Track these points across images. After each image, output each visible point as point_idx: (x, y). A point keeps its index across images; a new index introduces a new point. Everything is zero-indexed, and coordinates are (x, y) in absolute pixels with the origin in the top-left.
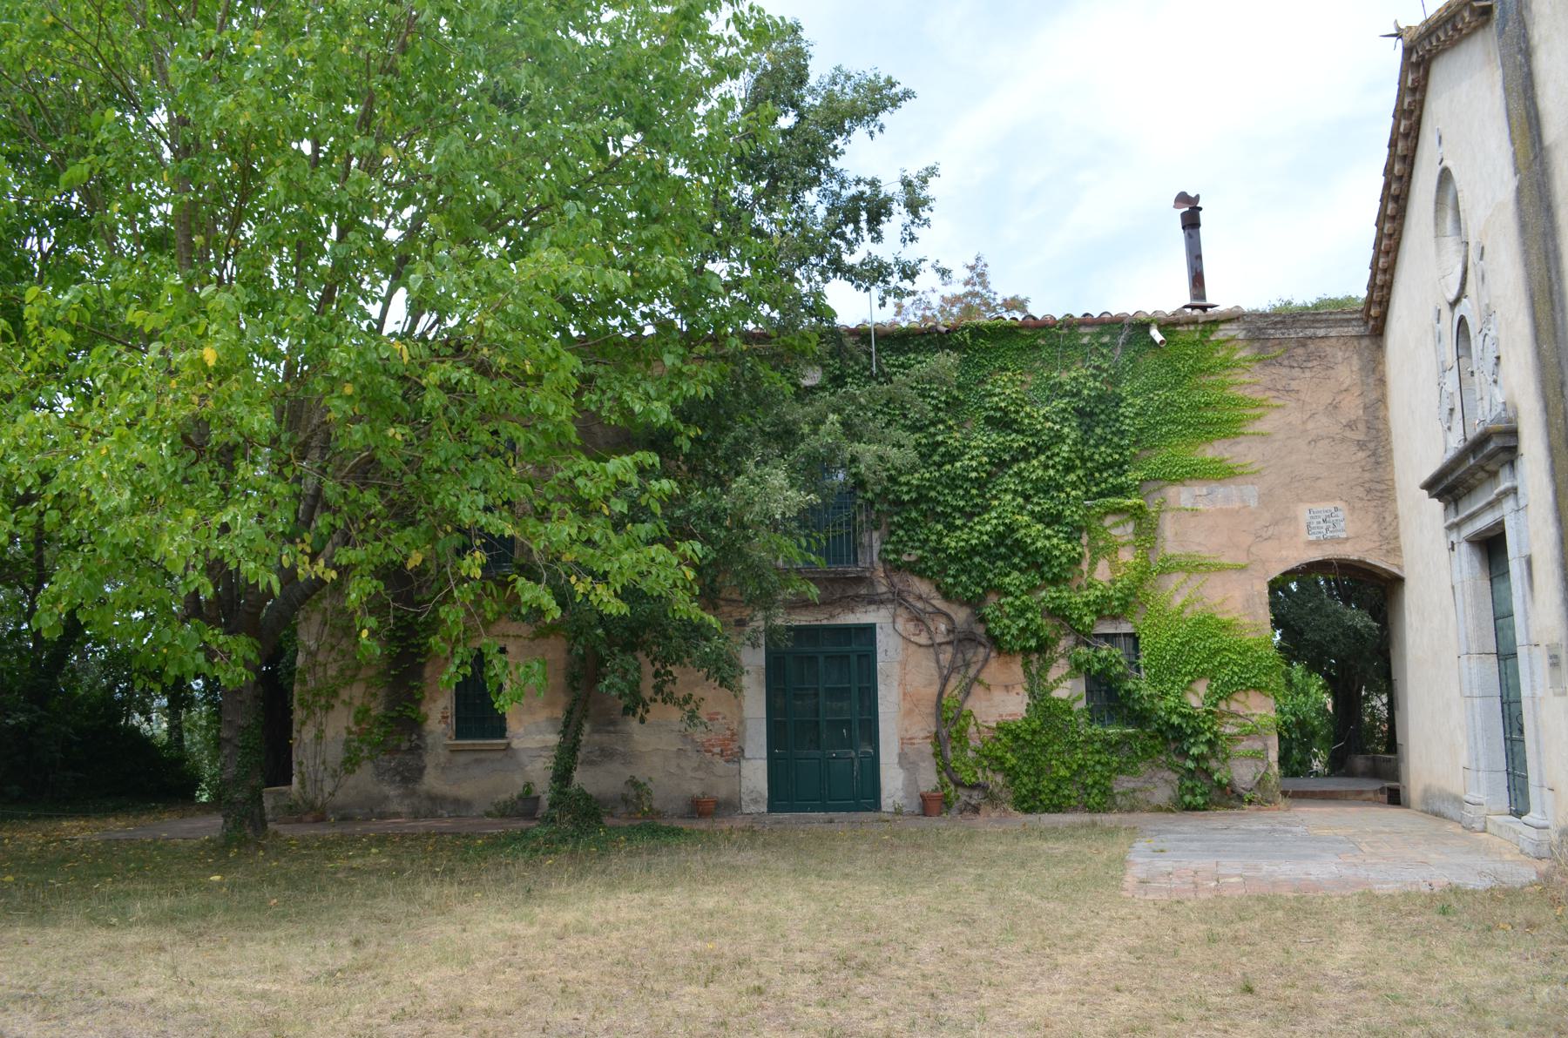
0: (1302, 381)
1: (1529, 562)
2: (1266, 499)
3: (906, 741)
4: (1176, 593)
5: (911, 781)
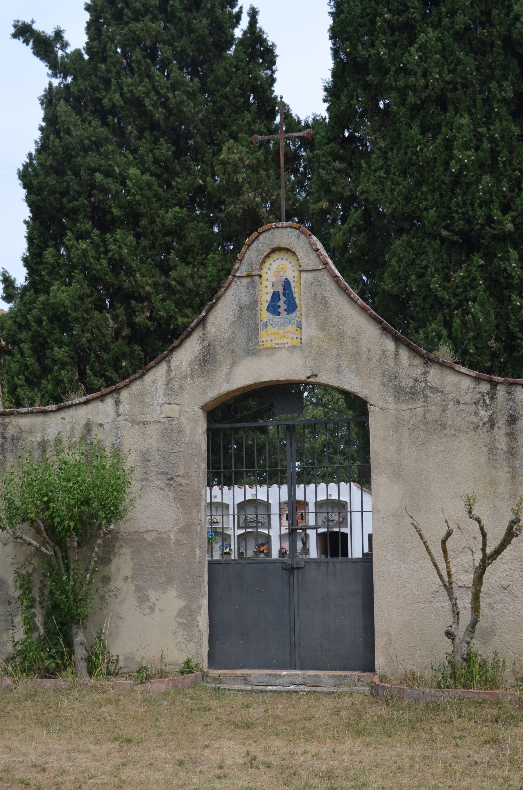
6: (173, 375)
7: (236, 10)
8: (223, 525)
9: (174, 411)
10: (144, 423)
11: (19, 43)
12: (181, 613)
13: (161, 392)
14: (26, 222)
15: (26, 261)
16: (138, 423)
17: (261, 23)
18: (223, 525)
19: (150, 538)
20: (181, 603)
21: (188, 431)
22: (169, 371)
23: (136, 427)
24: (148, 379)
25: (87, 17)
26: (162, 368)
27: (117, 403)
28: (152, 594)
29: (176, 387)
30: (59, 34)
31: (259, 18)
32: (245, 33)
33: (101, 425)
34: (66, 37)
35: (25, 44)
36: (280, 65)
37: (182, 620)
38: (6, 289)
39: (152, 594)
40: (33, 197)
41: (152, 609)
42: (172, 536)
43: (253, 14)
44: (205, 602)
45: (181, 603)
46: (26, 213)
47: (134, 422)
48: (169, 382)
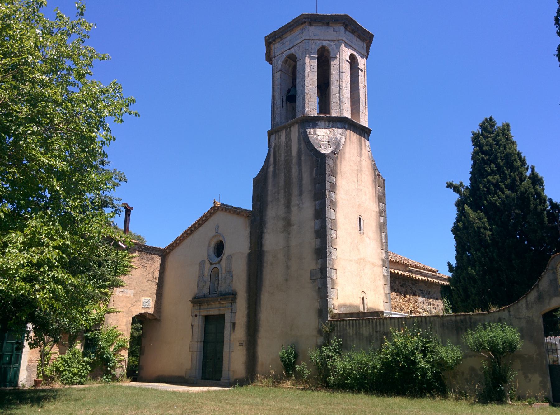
0: (148, 264)
1: (234, 325)
2: (135, 294)
3: (30, 361)
4: (111, 321)
5: (29, 376)
6: (528, 303)
7: (526, 166)
8: (230, 350)
10: (520, 318)
11: (448, 189)
12: (541, 382)
13: (525, 308)
14: (455, 246)
15: (456, 258)
16: (518, 318)
17: (536, 170)
18: (230, 350)
19: (526, 356)
20: (541, 379)
21: (536, 321)
22: (527, 301)
23: (517, 320)
24: (519, 304)
26: (524, 300)
27: (509, 312)
28: (530, 376)
29: (530, 307)
30: (461, 184)
31: (535, 169)
32: (530, 175)
33: (504, 319)
34: (464, 184)
35: (446, 185)
36: (545, 184)
37: (542, 385)
38: (449, 268)
39: (530, 376)
40: (456, 238)
41: (530, 380)
42: (534, 356)
43: (533, 169)
44: (549, 378)
45: (541, 379)
46: (454, 242)
47: (516, 318)
48: (527, 305)
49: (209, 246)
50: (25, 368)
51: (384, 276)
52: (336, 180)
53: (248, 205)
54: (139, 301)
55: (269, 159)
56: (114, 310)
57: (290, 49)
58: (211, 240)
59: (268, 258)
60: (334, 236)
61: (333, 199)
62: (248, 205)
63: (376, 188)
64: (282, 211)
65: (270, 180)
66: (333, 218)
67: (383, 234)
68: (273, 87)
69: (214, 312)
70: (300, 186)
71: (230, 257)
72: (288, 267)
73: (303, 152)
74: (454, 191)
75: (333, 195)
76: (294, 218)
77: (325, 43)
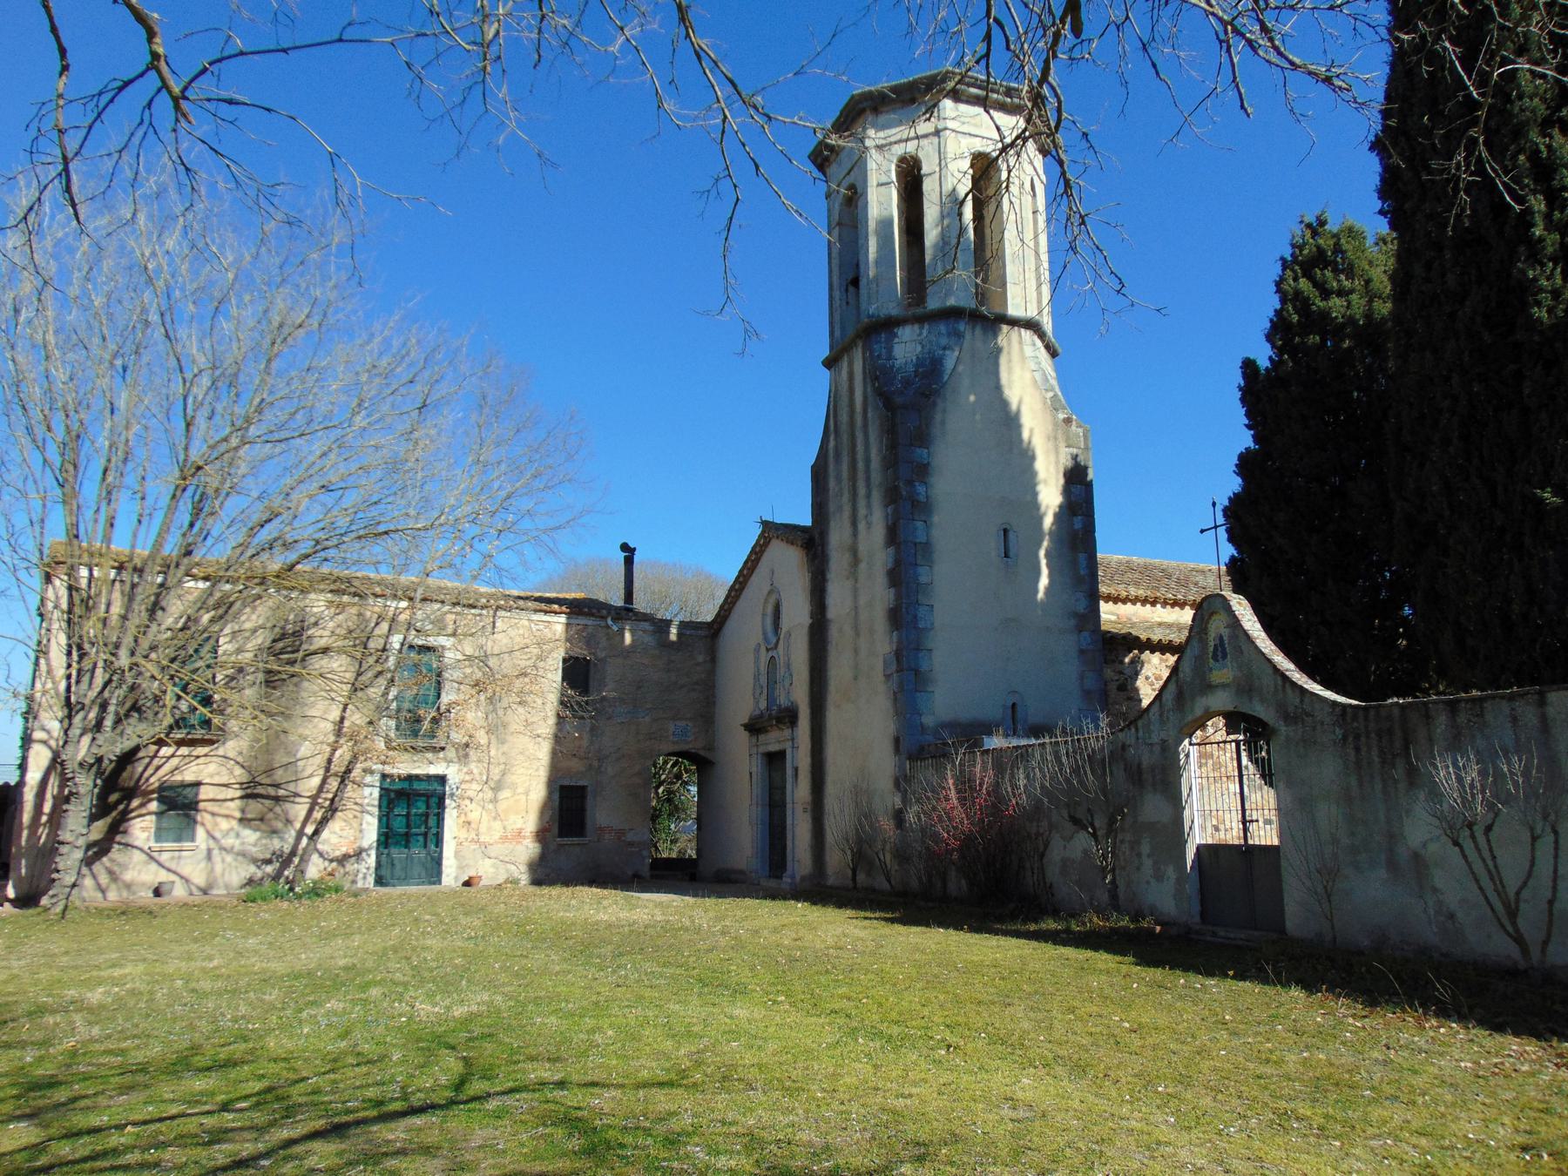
9: (1163, 735)
25: (1239, 394)
49: (764, 615)
50: (452, 854)
51: (1082, 652)
52: (929, 453)
53: (806, 521)
54: (1419, 861)
55: (828, 441)
56: (1363, 739)
57: (848, 174)
58: (766, 601)
59: (833, 633)
60: (923, 579)
61: (922, 498)
62: (806, 521)
63: (1057, 452)
64: (848, 531)
65: (831, 467)
66: (922, 538)
67: (1082, 557)
68: (830, 254)
69: (773, 748)
70: (868, 479)
71: (789, 634)
72: (856, 651)
73: (870, 399)
74: (125, 1171)
75: (921, 489)
76: (862, 548)
77: (911, 147)
